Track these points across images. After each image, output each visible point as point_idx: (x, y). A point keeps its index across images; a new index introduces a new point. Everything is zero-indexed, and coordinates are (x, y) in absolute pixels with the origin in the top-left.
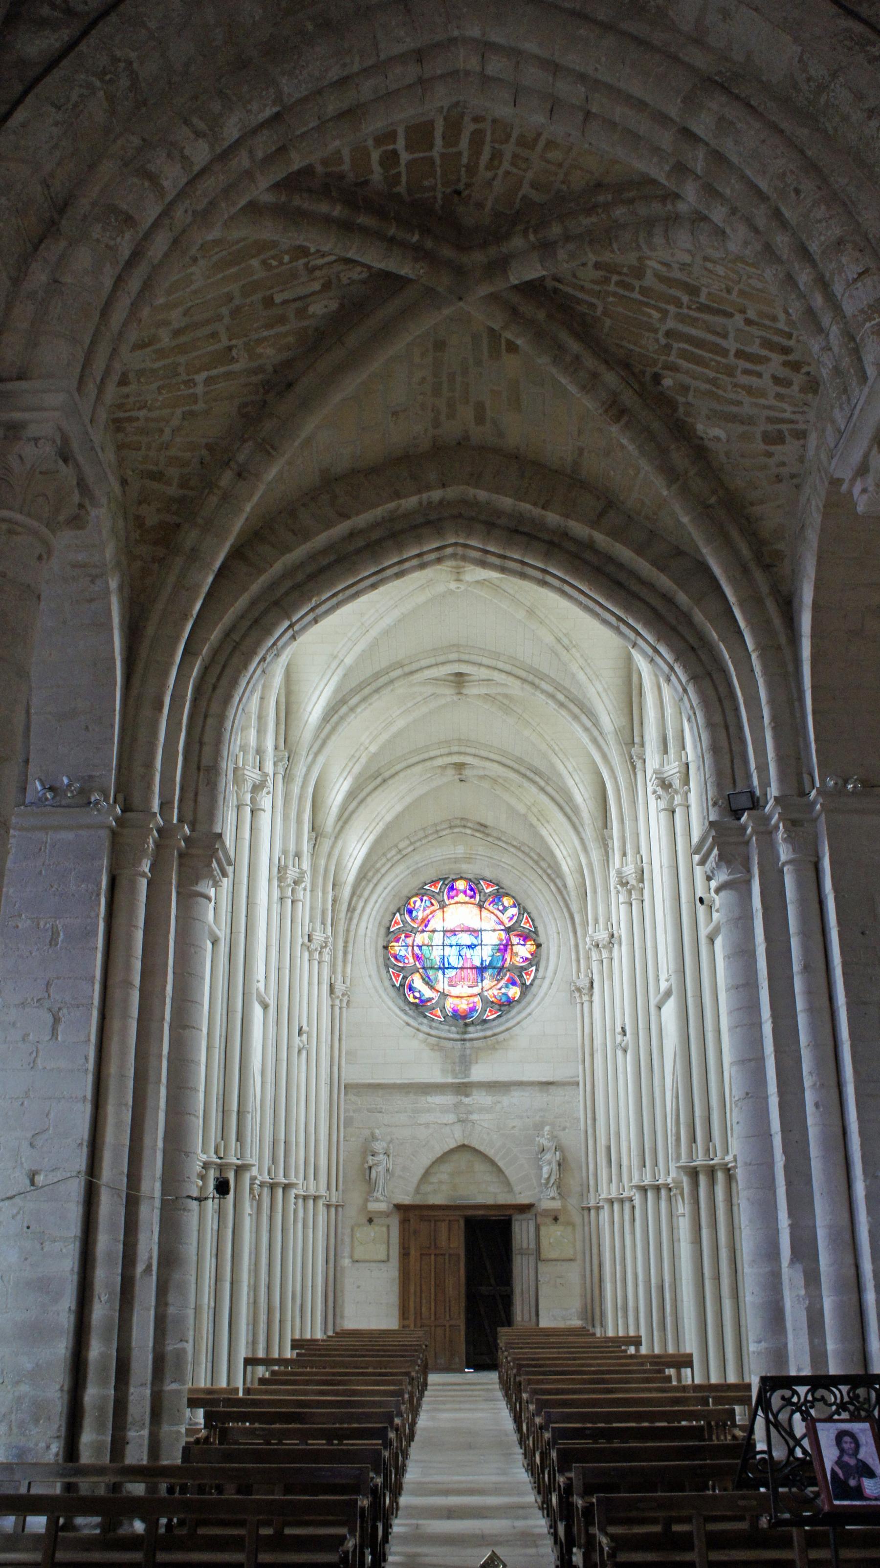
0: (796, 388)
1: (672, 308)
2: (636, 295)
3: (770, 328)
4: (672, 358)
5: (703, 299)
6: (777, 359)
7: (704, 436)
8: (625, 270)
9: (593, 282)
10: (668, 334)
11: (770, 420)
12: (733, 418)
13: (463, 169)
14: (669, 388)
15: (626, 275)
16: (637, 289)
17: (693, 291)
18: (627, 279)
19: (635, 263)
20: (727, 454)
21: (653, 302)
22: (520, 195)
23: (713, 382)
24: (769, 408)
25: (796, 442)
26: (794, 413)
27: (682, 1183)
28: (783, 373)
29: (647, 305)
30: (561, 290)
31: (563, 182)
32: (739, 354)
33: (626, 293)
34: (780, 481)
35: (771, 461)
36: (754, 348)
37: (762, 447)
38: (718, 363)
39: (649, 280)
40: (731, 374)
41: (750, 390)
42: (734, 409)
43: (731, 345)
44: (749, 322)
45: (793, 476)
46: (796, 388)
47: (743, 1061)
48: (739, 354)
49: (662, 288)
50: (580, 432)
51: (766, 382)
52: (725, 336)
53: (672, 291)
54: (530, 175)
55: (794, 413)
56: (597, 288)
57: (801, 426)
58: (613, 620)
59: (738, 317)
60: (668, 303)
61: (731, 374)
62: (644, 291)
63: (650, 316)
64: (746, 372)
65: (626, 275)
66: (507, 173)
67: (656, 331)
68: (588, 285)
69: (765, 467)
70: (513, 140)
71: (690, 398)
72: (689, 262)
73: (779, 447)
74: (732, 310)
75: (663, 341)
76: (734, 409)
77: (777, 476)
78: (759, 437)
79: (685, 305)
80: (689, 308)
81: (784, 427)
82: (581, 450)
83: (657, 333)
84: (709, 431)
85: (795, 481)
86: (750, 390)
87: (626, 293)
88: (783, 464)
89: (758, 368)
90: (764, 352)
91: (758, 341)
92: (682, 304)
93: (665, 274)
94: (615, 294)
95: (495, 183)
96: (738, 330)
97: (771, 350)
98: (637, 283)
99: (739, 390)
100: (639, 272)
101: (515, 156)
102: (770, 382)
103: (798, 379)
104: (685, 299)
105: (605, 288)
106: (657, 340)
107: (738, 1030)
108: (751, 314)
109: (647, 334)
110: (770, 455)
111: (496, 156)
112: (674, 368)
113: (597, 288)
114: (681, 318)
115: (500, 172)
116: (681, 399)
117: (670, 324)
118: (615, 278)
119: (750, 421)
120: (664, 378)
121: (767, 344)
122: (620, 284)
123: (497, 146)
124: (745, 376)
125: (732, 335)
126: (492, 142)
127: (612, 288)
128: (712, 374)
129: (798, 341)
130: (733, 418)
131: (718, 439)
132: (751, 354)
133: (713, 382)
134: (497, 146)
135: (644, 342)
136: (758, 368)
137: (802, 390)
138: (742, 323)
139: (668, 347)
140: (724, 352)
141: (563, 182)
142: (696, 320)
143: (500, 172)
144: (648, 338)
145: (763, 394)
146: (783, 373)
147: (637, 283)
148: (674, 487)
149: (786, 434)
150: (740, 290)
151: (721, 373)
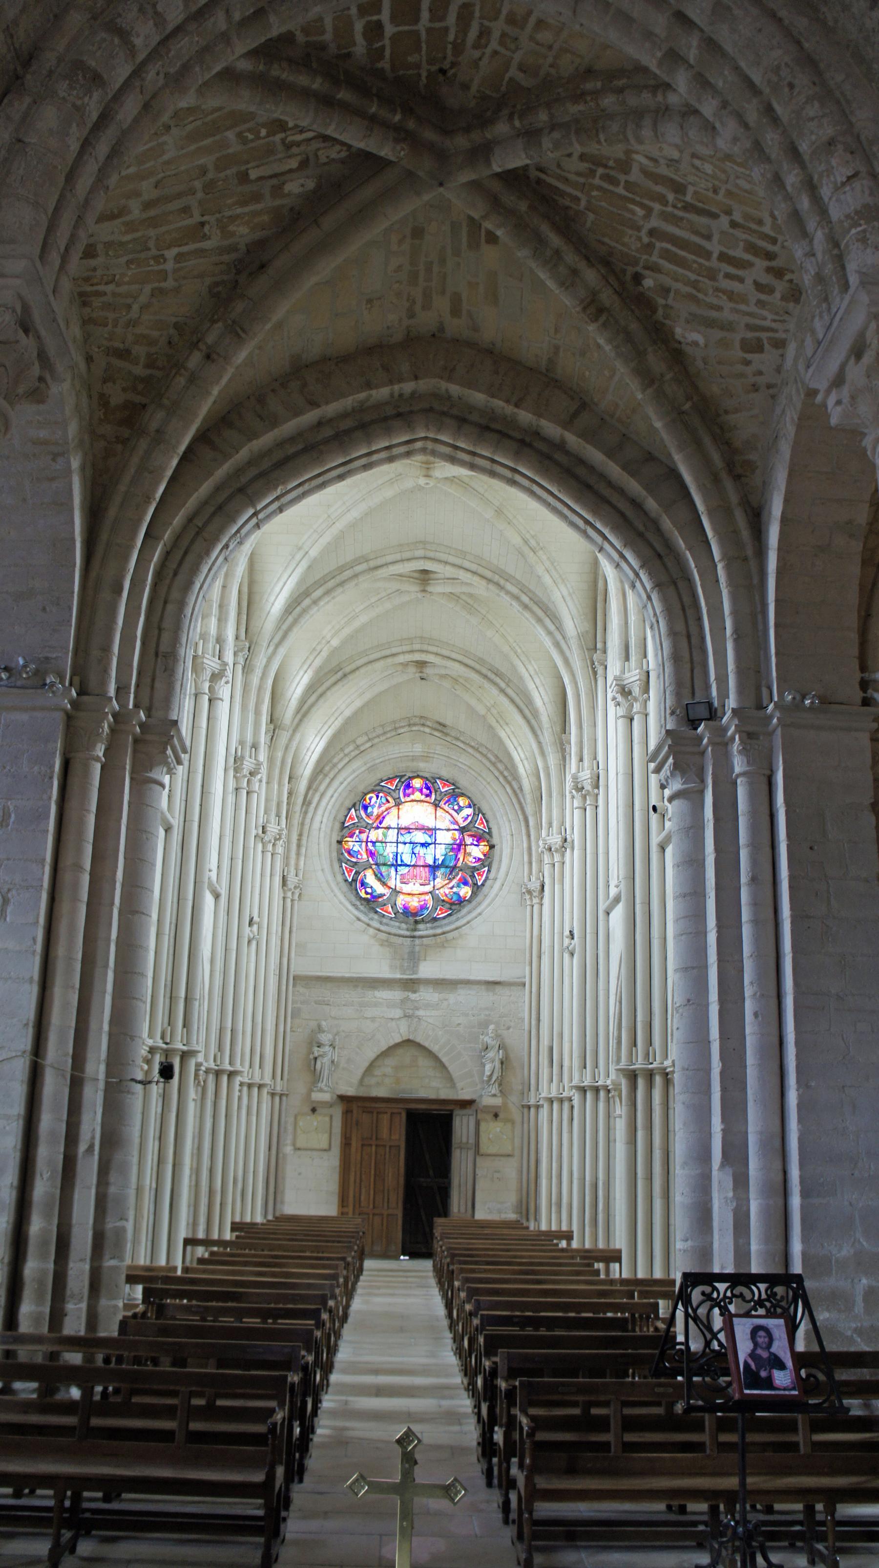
0: (778, 295)
1: (657, 207)
2: (620, 190)
3: (755, 231)
5: (688, 198)
6: (760, 264)
7: (682, 340)
9: (578, 174)
10: (652, 233)
12: (711, 323)
14: (649, 288)
15: (612, 168)
16: (622, 184)
17: (679, 189)
19: (621, 155)
22: (506, 78)
23: (695, 285)
26: (775, 321)
28: (766, 279)
31: (551, 66)
33: (611, 188)
34: (757, 390)
35: (749, 370)
36: (738, 253)
37: (741, 354)
38: (700, 265)
39: (635, 176)
41: (731, 296)
42: (714, 314)
43: (715, 247)
44: (734, 224)
51: (747, 288)
52: (708, 238)
53: (659, 189)
54: (518, 57)
55: (775, 321)
56: (582, 180)
57: (781, 335)
60: (653, 199)
62: (629, 186)
63: (633, 213)
64: (728, 276)
65: (612, 168)
66: (496, 53)
67: (639, 229)
68: (573, 177)
69: (742, 375)
71: (670, 301)
74: (717, 211)
75: (646, 240)
76: (714, 314)
77: (754, 385)
78: (737, 345)
80: (674, 206)
81: (764, 335)
82: (557, 348)
84: (687, 335)
85: (771, 391)
87: (611, 188)
88: (760, 373)
89: (740, 273)
91: (742, 244)
94: (600, 188)
97: (756, 255)
98: (622, 178)
99: (720, 294)
100: (624, 166)
101: (504, 35)
103: (780, 287)
104: (671, 197)
105: (590, 180)
106: (639, 239)
108: (737, 217)
109: (630, 232)
111: (484, 33)
112: (654, 268)
114: (666, 217)
115: (488, 51)
116: (661, 301)
117: (655, 222)
118: (600, 171)
119: (728, 327)
121: (751, 248)
122: (607, 178)
123: (486, 23)
125: (716, 238)
127: (597, 181)
128: (693, 277)
131: (695, 344)
134: (486, 23)
136: (740, 273)
140: (708, 255)
142: (682, 219)
146: (766, 279)
147: (622, 178)
148: (650, 391)
149: (765, 342)
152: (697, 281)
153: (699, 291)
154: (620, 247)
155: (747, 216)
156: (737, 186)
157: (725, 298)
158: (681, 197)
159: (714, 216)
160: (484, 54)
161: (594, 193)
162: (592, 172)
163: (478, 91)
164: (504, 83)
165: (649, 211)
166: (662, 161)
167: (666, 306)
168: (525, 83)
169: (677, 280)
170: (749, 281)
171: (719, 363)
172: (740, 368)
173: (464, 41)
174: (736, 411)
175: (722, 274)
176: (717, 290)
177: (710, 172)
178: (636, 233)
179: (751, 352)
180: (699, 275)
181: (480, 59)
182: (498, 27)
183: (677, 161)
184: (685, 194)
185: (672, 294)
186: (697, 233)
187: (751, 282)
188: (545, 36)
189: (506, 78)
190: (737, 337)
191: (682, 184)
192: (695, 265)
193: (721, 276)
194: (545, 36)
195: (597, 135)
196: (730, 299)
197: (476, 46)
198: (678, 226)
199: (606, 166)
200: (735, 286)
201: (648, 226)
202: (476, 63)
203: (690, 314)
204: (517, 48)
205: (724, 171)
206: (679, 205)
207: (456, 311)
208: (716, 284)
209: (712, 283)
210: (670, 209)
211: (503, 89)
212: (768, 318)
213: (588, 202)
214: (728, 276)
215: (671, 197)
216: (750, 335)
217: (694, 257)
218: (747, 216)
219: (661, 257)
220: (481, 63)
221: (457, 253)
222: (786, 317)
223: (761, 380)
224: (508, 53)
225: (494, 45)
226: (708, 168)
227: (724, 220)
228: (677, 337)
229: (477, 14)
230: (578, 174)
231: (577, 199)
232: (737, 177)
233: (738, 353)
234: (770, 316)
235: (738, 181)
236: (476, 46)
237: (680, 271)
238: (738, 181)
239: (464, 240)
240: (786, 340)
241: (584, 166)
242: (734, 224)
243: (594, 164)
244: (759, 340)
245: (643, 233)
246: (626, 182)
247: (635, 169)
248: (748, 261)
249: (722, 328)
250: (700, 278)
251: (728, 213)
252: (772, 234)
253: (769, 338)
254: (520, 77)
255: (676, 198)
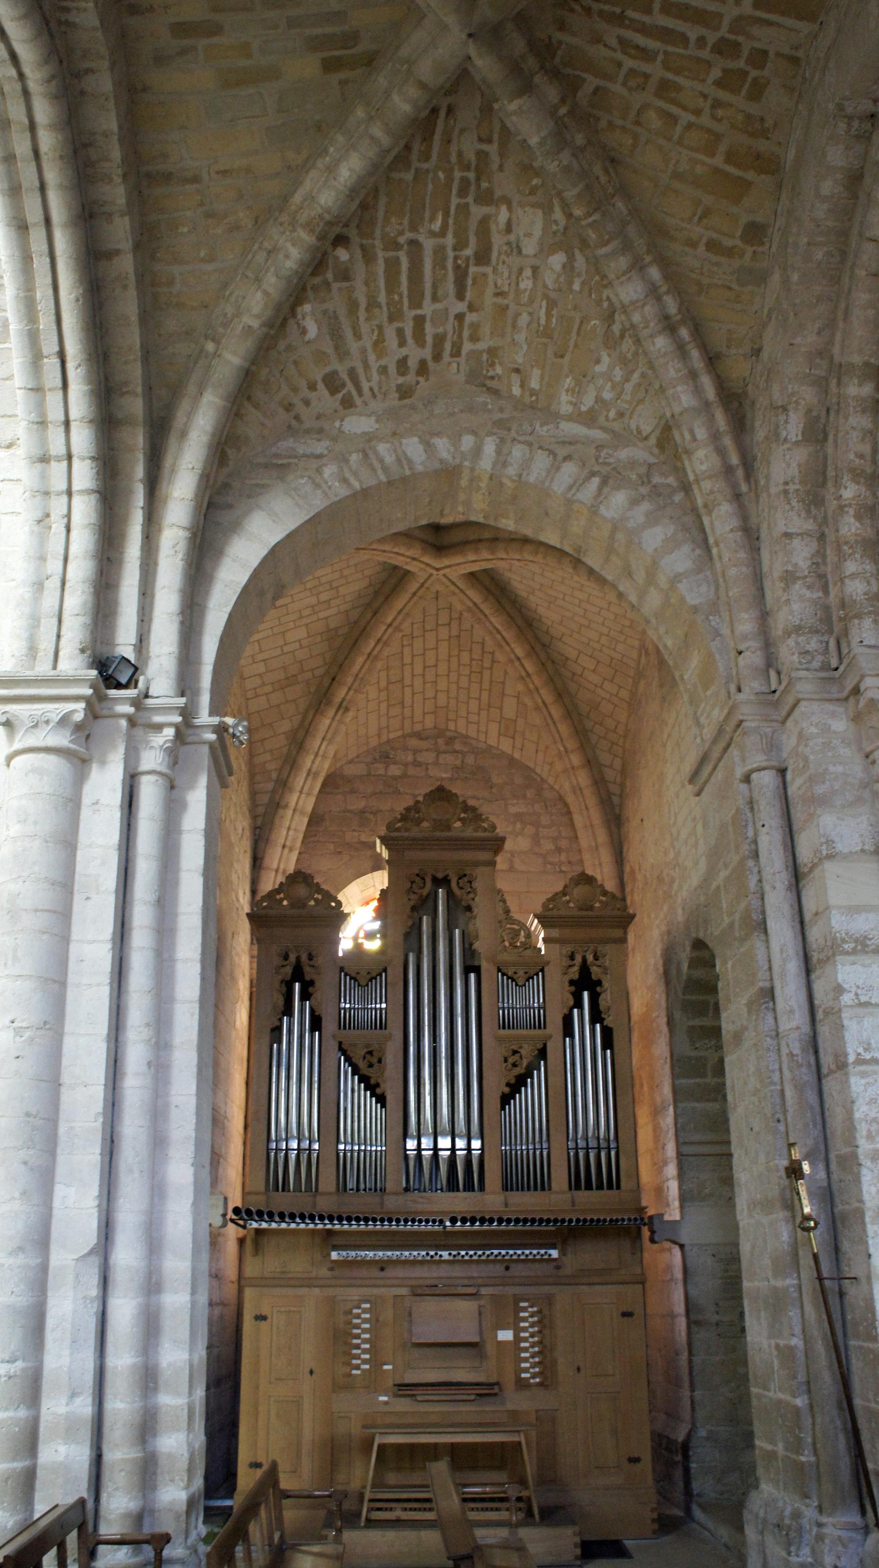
0: (401, 380)
1: (450, 240)
2: (455, 201)
3: (460, 336)
4: (380, 254)
5: (472, 270)
6: (427, 353)
7: (299, 317)
8: (485, 185)
9: (460, 154)
10: (414, 244)
11: (352, 373)
12: (336, 333)
13: (618, 10)
14: (337, 258)
15: (478, 186)
16: (463, 201)
17: (483, 257)
18: (473, 188)
19: (498, 193)
20: (289, 348)
21: (451, 221)
22: (584, 75)
23: (372, 304)
24: (367, 367)
25: (338, 403)
26: (371, 389)
27: (684, 1198)
28: (413, 363)
29: (446, 215)
30: (437, 117)
31: (610, 123)
32: (419, 321)
33: (454, 192)
34: (288, 410)
35: (305, 392)
36: (429, 330)
37: (319, 377)
38: (401, 301)
39: (477, 211)
40: (391, 319)
41: (379, 343)
42: (348, 333)
43: (428, 308)
44: (460, 317)
45: (297, 418)
46: (401, 380)
47: (46, 979)
48: (419, 321)
49: (473, 225)
50: (224, 173)
51: (394, 351)
52: (435, 299)
53: (473, 240)
54: (617, 88)
55: (371, 389)
56: (454, 159)
57: (358, 401)
58: (50, 346)
59: (461, 307)
60: (456, 235)
61: (391, 319)
62: (464, 209)
63: (432, 219)
64: (400, 332)
65: (478, 186)
66: (620, 65)
67: (413, 228)
68: (454, 149)
69: (295, 390)
70: (670, 76)
71: (335, 286)
72: (524, 252)
73: (326, 393)
74: (468, 298)
75: (402, 240)
76: (348, 333)
77: (290, 405)
78: (328, 370)
79: (457, 253)
80: (456, 258)
81: (350, 387)
82: (196, 179)
83: (410, 231)
84: (308, 318)
85: (294, 423)
86: (379, 343)
87: (454, 192)
88: (307, 403)
89: (410, 341)
90: (429, 340)
91: (441, 330)
92: (461, 250)
93: (493, 227)
94: (450, 179)
95: (601, 47)
96: (447, 309)
97: (435, 346)
98: (470, 199)
99: (376, 333)
100: (486, 198)
101: (647, 76)
102: (399, 356)
103: (410, 378)
104: (469, 252)
105: (456, 168)
106: (401, 233)
107: (45, 937)
108: (470, 318)
109: (406, 222)
110: (312, 387)
111: (646, 55)
112: (368, 257)
113: (454, 159)
114: (439, 253)
115: (619, 56)
116: (330, 276)
117: (429, 245)
118: (471, 175)
119: (342, 353)
120: (346, 248)
121: (439, 340)
122: (465, 182)
123: (660, 57)
124: (394, 334)
125: (438, 306)
126: (666, 53)
127: (457, 174)
128: (382, 298)
129: (450, 363)
130: (336, 333)
131: (304, 332)
132: (424, 329)
133: (372, 304)
134: (660, 57)
135: (393, 220)
136: (410, 341)
137: (399, 388)
138: (457, 311)
139: (397, 247)
140: (416, 303)
141: (610, 123)
142: (444, 267)
143: (619, 56)
144: (401, 224)
145: (381, 355)
146: (413, 363)
147: (470, 199)
148: (265, 330)
149: (344, 392)
150: (507, 307)
151: (388, 309)
152: (379, 306)
153: (367, 310)
154: (381, 214)
155: (475, 327)
156: (517, 315)
157: (375, 338)
158: (471, 262)
159: (460, 296)
160: (614, 50)
161: (441, 175)
162: (468, 168)
163: (560, 43)
164: (577, 73)
165: (443, 233)
166: (512, 237)
167: (328, 284)
168: (580, 94)
169: (367, 284)
170: (404, 351)
171: (295, 363)
172: (303, 384)
173: (628, 27)
174: (257, 406)
175: (400, 325)
176: (380, 328)
177: (522, 286)
178: (407, 227)
179: (326, 385)
180: (388, 304)
181: (605, 45)
182: (656, 70)
183: (520, 252)
184: (476, 265)
185: (345, 284)
186: (435, 287)
187: (404, 354)
188: (653, 120)
189: (584, 75)
190: (336, 365)
191: (490, 260)
192: (396, 297)
193: (396, 325)
194: (653, 120)
195: (596, 210)
196: (376, 344)
197: (621, 41)
198: (434, 267)
199: (478, 179)
200: (392, 341)
201: (421, 238)
202: (597, 39)
203: (335, 312)
204: (630, 89)
205: (531, 301)
206: (459, 262)
207: (181, 29)
208: (386, 324)
209: (385, 319)
210: (451, 254)
211: (569, 71)
212: (371, 381)
213: (427, 171)
214: (400, 332)
215: (469, 252)
216: (345, 377)
217: (405, 293)
218: (475, 327)
219: (386, 260)
220: (601, 47)
221: (293, 23)
222: (380, 397)
223: (300, 408)
224: (621, 78)
225: (629, 63)
226: (526, 284)
227: (461, 307)
228: (299, 309)
229: (670, 49)
230: (460, 154)
231: (426, 157)
232: (530, 314)
233: (318, 375)
234: (374, 384)
235: (525, 315)
236: (621, 41)
237: (382, 283)
238: (525, 315)
239: (318, 31)
240: (356, 406)
241: (471, 157)
242: (460, 317)
243: (477, 167)
244: (344, 385)
245: (409, 235)
246: (467, 204)
247: (486, 210)
248: (425, 342)
249: (337, 348)
250: (385, 309)
251: (471, 308)
252: (464, 352)
253: (349, 393)
254: (587, 89)
255: (467, 259)
